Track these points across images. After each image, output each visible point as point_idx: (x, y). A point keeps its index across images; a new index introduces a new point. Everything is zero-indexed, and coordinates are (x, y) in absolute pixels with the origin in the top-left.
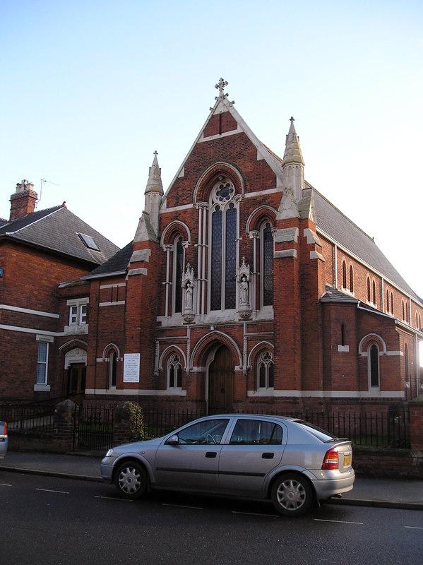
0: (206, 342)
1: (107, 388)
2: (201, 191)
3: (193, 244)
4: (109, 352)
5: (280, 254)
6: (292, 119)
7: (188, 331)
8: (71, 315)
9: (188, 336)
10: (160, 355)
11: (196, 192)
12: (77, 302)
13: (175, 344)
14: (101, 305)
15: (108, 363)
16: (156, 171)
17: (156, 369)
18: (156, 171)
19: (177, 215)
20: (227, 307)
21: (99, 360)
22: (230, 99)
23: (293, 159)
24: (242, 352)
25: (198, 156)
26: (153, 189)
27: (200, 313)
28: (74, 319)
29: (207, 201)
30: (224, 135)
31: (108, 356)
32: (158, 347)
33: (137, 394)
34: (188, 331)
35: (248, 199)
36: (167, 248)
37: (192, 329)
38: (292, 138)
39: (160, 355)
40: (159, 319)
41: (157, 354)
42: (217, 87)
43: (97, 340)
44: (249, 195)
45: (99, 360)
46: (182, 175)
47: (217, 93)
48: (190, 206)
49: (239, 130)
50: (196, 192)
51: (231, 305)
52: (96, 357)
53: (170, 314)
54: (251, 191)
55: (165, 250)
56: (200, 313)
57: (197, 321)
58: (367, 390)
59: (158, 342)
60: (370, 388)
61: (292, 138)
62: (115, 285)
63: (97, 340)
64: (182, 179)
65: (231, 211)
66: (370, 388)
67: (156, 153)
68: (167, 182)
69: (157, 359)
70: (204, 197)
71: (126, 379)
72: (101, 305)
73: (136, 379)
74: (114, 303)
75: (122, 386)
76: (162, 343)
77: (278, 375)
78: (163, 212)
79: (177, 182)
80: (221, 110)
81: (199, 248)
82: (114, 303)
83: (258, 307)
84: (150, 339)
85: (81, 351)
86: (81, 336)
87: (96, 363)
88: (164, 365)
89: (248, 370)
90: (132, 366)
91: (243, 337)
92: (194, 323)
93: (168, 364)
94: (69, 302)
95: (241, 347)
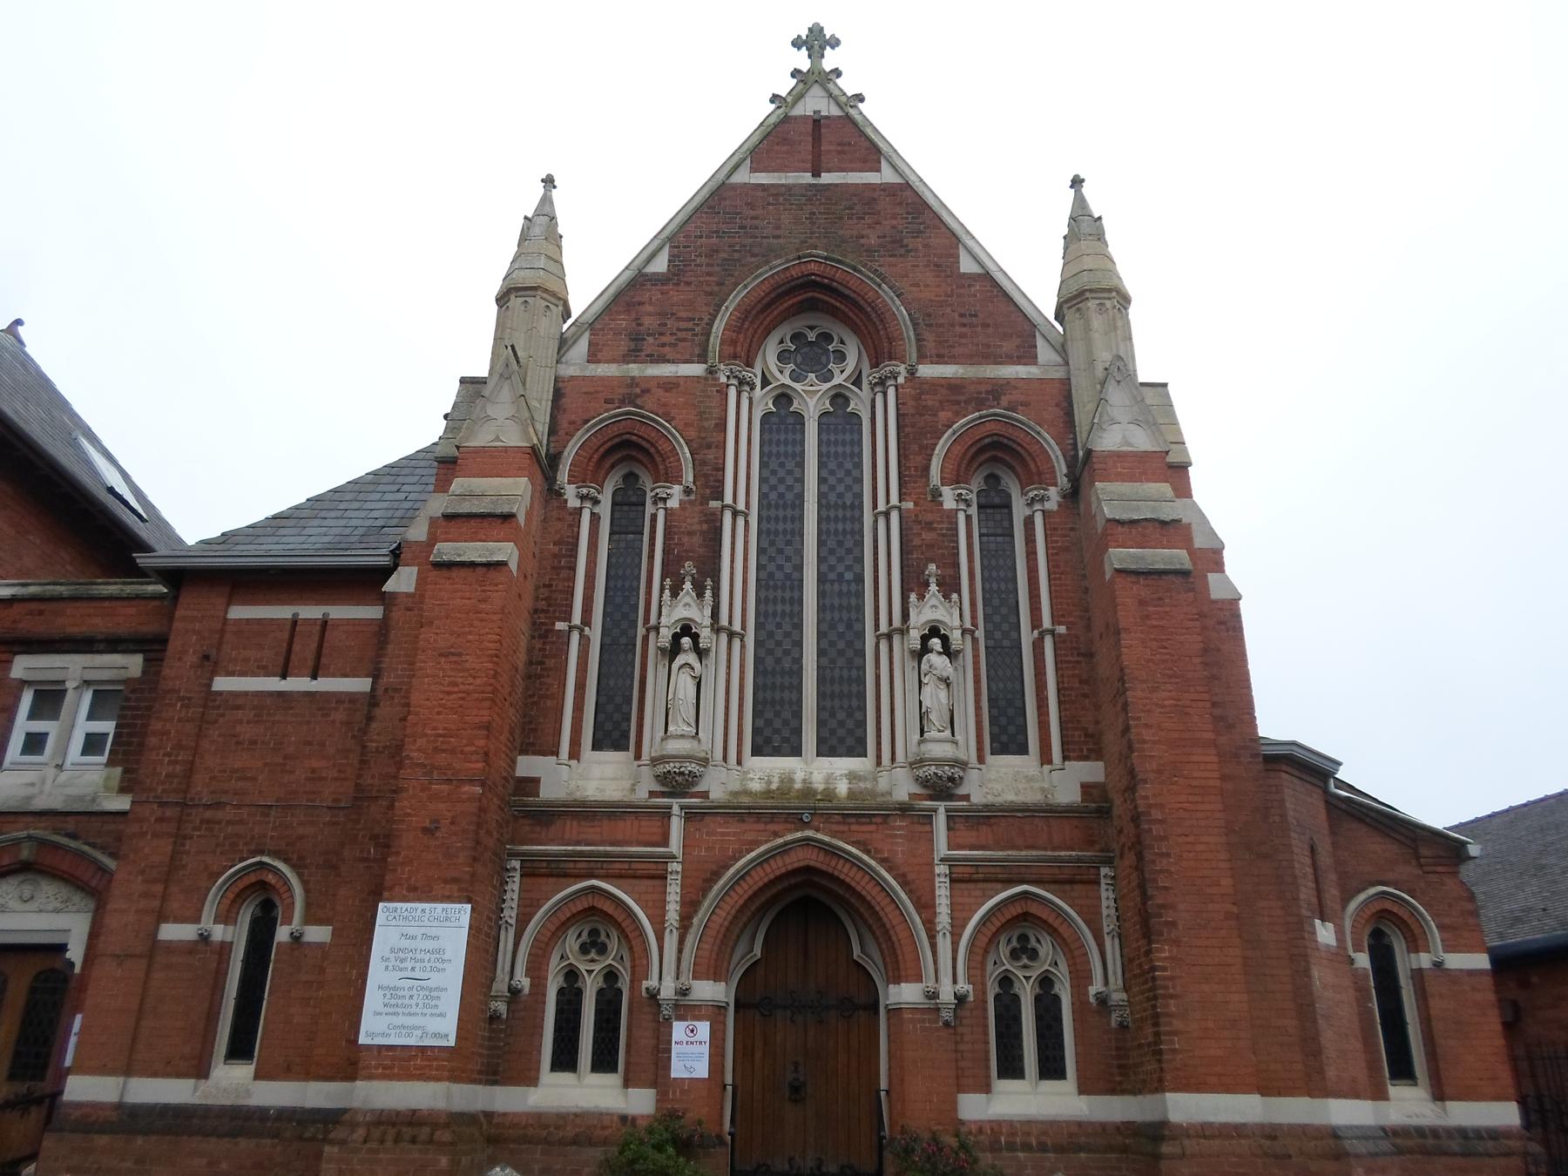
0: (759, 878)
1: (201, 1070)
2: (736, 328)
3: (704, 501)
4: (240, 897)
5: (1143, 558)
6: (1077, 182)
7: (676, 826)
8: (22, 725)
9: (675, 845)
10: (522, 922)
11: (719, 327)
12: (71, 667)
13: (605, 877)
14: (222, 684)
15: (225, 948)
16: (541, 234)
17: (500, 986)
18: (541, 234)
19: (634, 391)
20: (827, 748)
21: (172, 932)
22: (848, 85)
23: (1093, 292)
24: (930, 925)
25: (715, 226)
26: (529, 290)
27: (725, 759)
28: (34, 743)
29: (750, 364)
30: (827, 178)
31: (226, 917)
32: (514, 886)
33: (441, 1104)
34: (676, 826)
35: (935, 384)
36: (583, 498)
37: (691, 816)
38: (1084, 230)
39: (522, 922)
40: (527, 765)
41: (510, 914)
42: (797, 43)
43: (180, 838)
44: (927, 371)
45: (172, 932)
46: (660, 265)
47: (802, 61)
48: (696, 369)
49: (886, 176)
50: (719, 327)
51: (842, 737)
52: (162, 917)
53: (575, 754)
54: (940, 359)
55: (573, 502)
56: (725, 759)
57: (718, 785)
58: (986, 1089)
59: (516, 864)
60: (547, 1077)
61: (1084, 230)
62: (311, 612)
63: (180, 838)
64: (657, 280)
65: (841, 422)
66: (547, 1077)
67: (549, 182)
68: (588, 279)
69: (507, 939)
70: (743, 349)
71: (378, 1025)
72: (222, 684)
73: (439, 1024)
74: (297, 684)
75: (351, 1061)
76: (531, 871)
77: (1177, 1024)
78: (567, 371)
79: (631, 293)
80: (815, 103)
81: (728, 516)
82: (297, 684)
83: (981, 759)
84: (506, 846)
85: (49, 891)
86: (79, 820)
87: (155, 947)
88: (536, 969)
89: (960, 999)
90: (417, 968)
91: (931, 865)
92: (705, 795)
93: (554, 967)
94: (22, 666)
95: (926, 906)
